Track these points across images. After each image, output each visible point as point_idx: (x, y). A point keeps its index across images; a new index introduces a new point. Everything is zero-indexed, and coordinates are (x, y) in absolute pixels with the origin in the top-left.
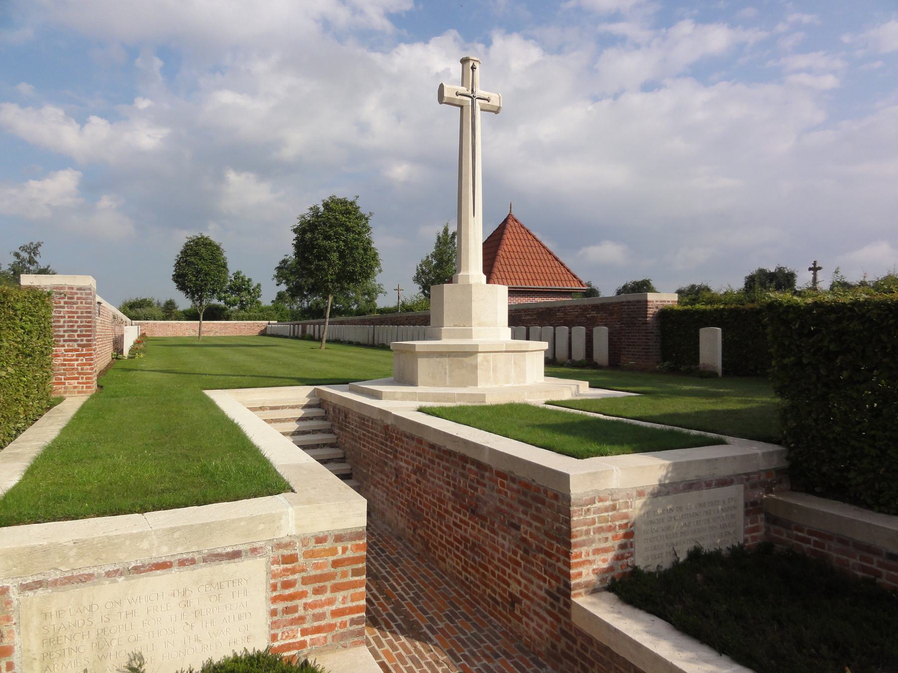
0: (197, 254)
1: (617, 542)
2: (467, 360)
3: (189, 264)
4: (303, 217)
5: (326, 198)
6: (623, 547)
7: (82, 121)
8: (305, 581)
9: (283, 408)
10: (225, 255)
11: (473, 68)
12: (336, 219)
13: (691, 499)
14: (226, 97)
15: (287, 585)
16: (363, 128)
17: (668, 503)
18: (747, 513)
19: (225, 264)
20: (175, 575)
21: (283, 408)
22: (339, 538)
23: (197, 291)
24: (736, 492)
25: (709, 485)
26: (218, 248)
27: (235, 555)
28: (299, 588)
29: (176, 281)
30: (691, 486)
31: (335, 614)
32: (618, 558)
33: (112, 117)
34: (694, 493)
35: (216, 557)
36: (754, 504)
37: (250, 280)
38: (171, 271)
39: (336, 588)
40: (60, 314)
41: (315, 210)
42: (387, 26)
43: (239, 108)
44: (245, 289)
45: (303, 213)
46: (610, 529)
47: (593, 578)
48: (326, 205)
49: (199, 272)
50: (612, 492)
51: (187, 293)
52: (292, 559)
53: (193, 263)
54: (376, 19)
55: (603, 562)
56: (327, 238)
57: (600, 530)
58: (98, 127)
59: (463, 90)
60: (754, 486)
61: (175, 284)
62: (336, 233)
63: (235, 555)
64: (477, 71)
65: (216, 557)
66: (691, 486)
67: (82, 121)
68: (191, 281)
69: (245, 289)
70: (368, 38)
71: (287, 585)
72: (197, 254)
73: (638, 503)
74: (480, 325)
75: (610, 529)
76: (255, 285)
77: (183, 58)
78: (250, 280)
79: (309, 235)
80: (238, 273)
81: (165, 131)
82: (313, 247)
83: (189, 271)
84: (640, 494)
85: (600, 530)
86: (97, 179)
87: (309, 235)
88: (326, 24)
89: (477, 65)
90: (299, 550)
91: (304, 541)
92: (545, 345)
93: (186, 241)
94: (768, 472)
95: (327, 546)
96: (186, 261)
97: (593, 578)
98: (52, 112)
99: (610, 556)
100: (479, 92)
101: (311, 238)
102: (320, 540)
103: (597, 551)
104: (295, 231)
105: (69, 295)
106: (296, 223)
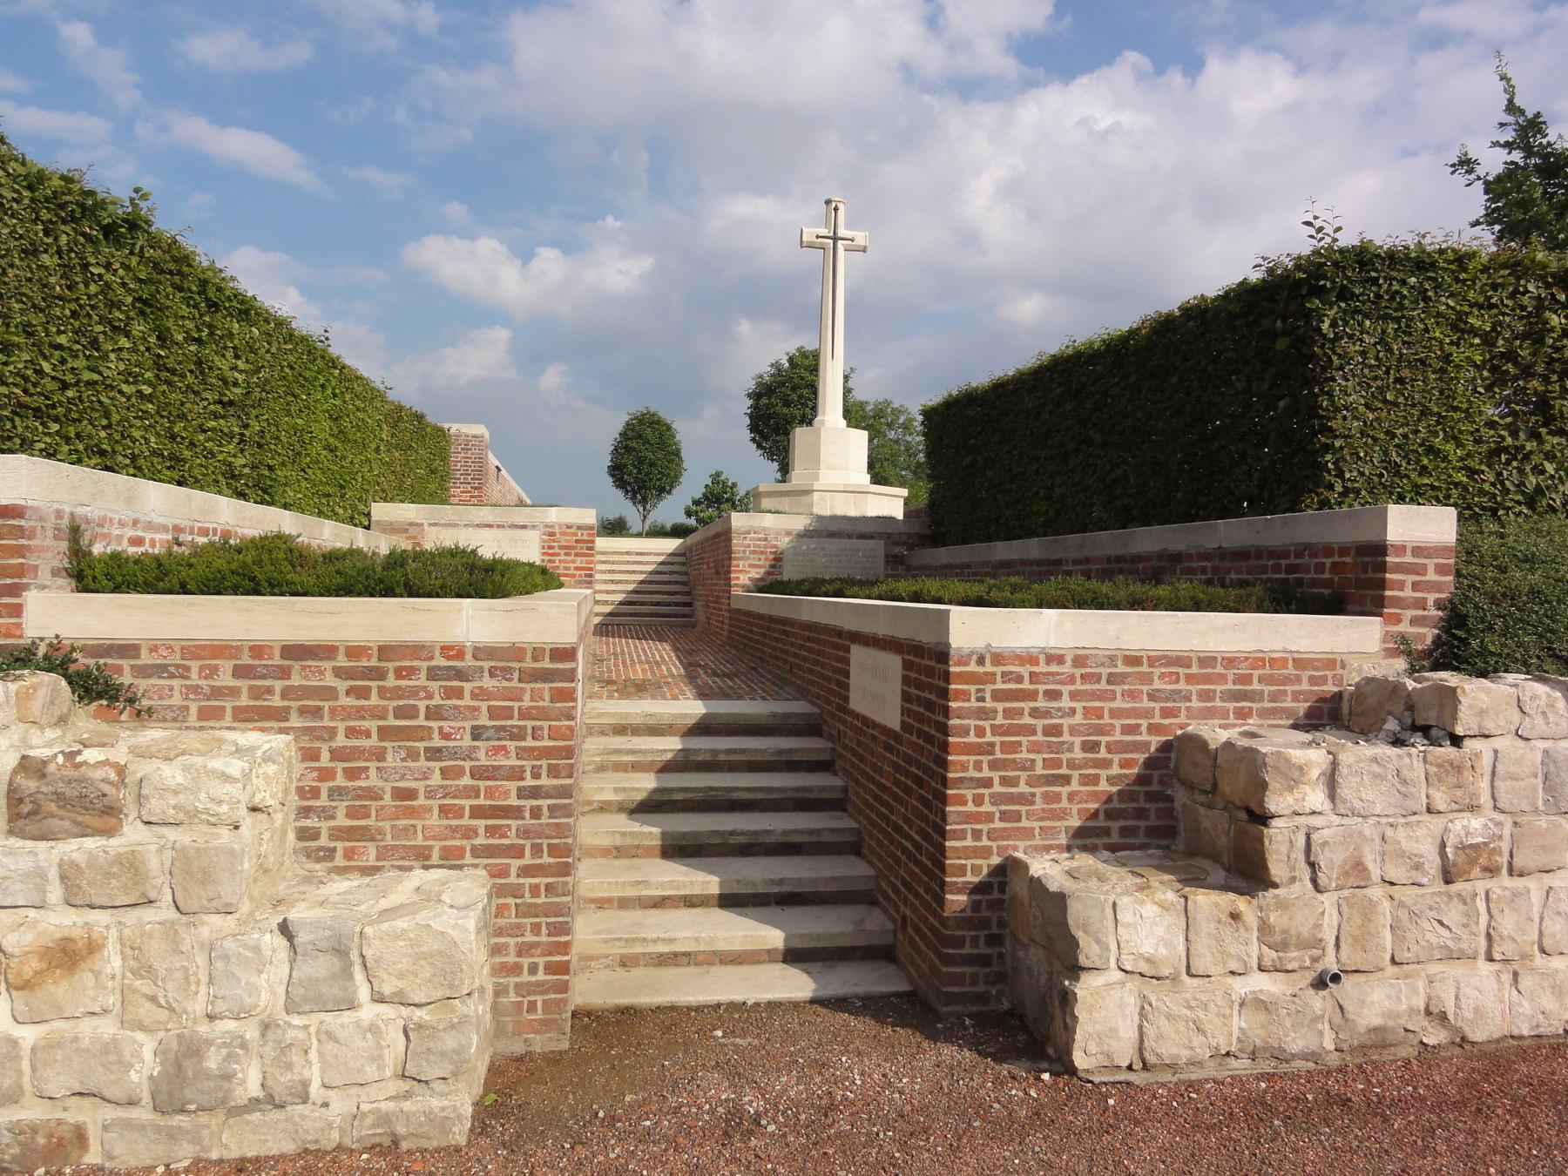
2: (803, 498)
13: (833, 544)
14: (744, 207)
15: (550, 547)
16: (970, 238)
17: (814, 543)
18: (887, 562)
20: (495, 530)
22: (579, 528)
23: (640, 488)
24: (878, 547)
25: (850, 536)
26: (669, 428)
27: (524, 527)
28: (556, 550)
30: (832, 535)
32: (768, 573)
33: (569, 246)
34: (836, 540)
36: (895, 556)
37: (734, 485)
38: (607, 461)
39: (577, 555)
40: (457, 458)
42: (1009, 67)
43: (764, 222)
44: (727, 500)
47: (748, 582)
48: (791, 360)
49: (641, 461)
50: (764, 529)
51: (627, 492)
52: (553, 534)
53: (634, 449)
54: (992, 58)
55: (756, 573)
56: (787, 404)
57: (754, 552)
58: (550, 261)
60: (895, 544)
62: (801, 396)
63: (524, 527)
66: (832, 535)
67: (524, 254)
68: (630, 474)
70: (970, 88)
71: (550, 547)
72: (640, 436)
73: (787, 539)
76: (742, 493)
78: (734, 485)
80: (718, 474)
81: (644, 263)
82: (770, 417)
83: (629, 460)
84: (788, 533)
85: (754, 552)
86: (540, 341)
87: (765, 401)
88: (908, 72)
90: (557, 530)
91: (560, 526)
92: (905, 492)
93: (627, 418)
94: (909, 535)
98: (488, 246)
99: (762, 571)
102: (569, 527)
104: (749, 395)
105: (470, 442)
106: (751, 385)
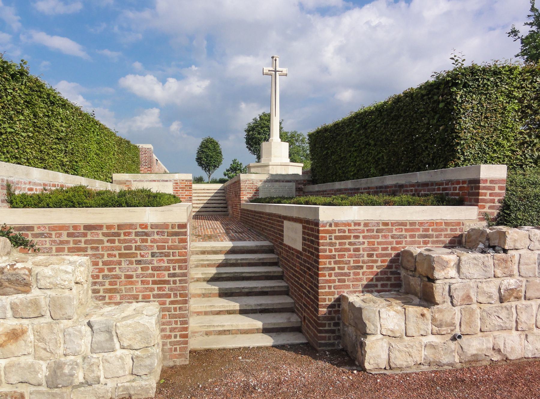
0: (207, 147)
1: (254, 192)
3: (203, 152)
4: (250, 124)
5: (261, 114)
6: (255, 193)
7: (163, 81)
8: (180, 188)
9: (211, 190)
10: (220, 147)
11: (276, 60)
12: (264, 124)
15: (176, 188)
16: (325, 69)
17: (270, 184)
18: (296, 191)
19: (221, 152)
21: (211, 190)
22: (186, 181)
24: (293, 185)
25: (283, 181)
26: (217, 144)
27: (167, 181)
28: (179, 189)
29: (198, 162)
31: (186, 195)
32: (254, 196)
33: (179, 77)
35: (163, 181)
37: (241, 164)
38: (195, 156)
39: (186, 191)
41: (255, 119)
44: (239, 169)
45: (249, 122)
46: (252, 188)
47: (247, 199)
48: (260, 117)
49: (208, 156)
50: (252, 180)
52: (177, 183)
53: (205, 152)
55: (250, 196)
57: (249, 188)
58: (172, 82)
59: (271, 69)
60: (299, 184)
61: (197, 163)
62: (264, 131)
63: (167, 181)
64: (277, 61)
65: (163, 181)
67: (163, 81)
68: (204, 161)
69: (239, 169)
71: (176, 188)
72: (207, 147)
73: (260, 183)
74: (275, 157)
75: (252, 188)
77: (212, 41)
78: (241, 164)
79: (251, 133)
80: (235, 160)
82: (253, 139)
83: (203, 156)
84: (261, 181)
85: (249, 188)
86: (170, 113)
89: (277, 59)
90: (178, 182)
91: (180, 180)
92: (302, 165)
93: (202, 140)
95: (184, 182)
96: (202, 151)
97: (247, 199)
98: (150, 78)
99: (252, 195)
100: (278, 69)
101: (252, 134)
103: (248, 193)
105: (146, 151)
106: (246, 127)
